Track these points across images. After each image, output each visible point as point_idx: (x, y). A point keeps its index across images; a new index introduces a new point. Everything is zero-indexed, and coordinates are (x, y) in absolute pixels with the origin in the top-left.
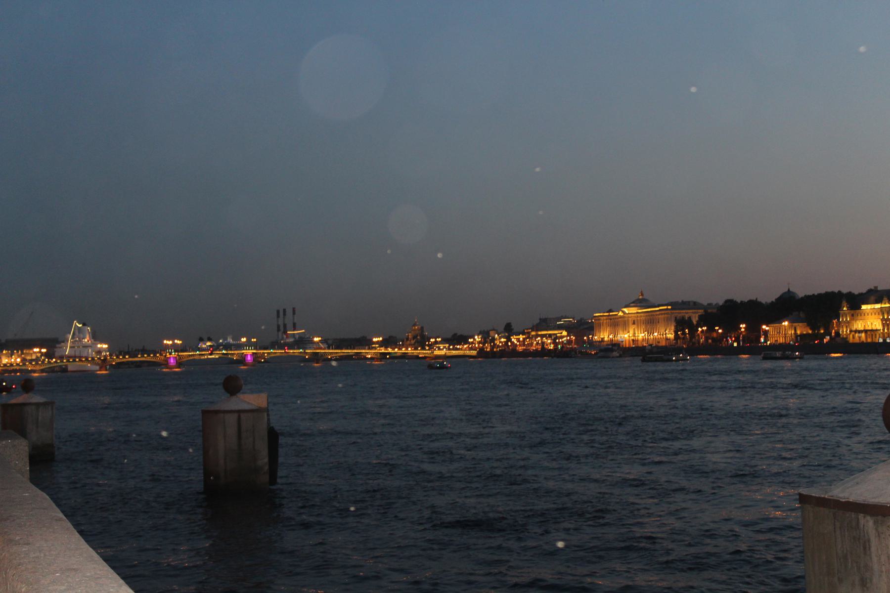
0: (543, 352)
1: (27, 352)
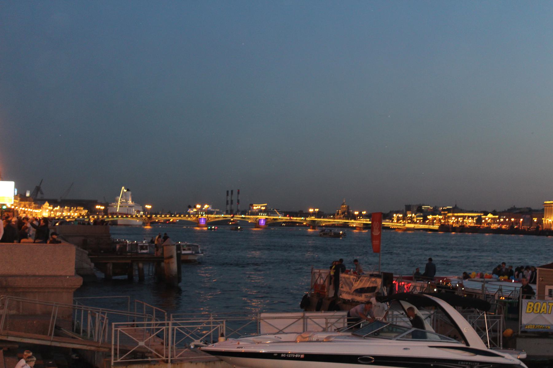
0: (463, 229)
1: (80, 209)
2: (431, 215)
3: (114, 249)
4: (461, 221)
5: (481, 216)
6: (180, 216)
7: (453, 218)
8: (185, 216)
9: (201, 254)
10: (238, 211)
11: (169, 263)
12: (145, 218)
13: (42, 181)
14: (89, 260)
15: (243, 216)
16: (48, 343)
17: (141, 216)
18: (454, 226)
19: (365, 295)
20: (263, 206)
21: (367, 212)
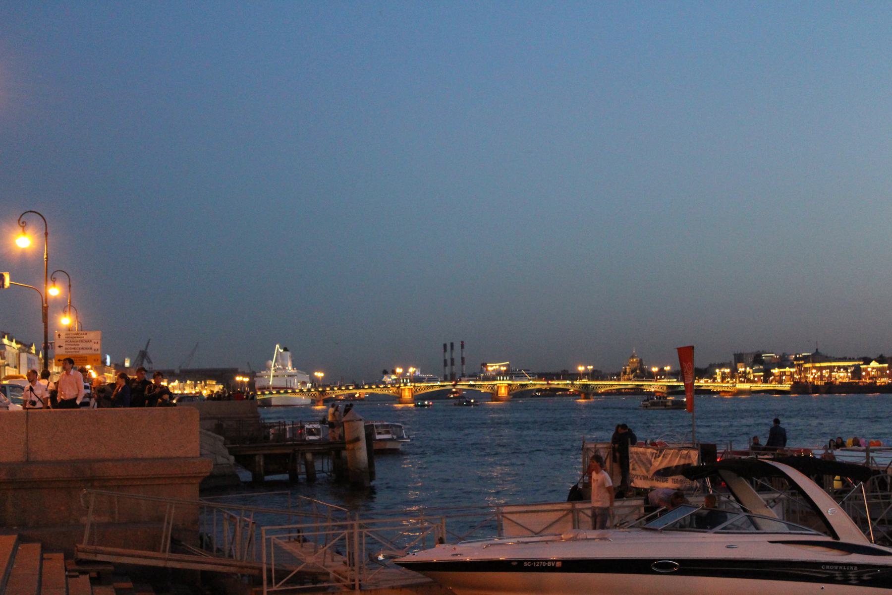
0: (831, 388)
1: (210, 383)
2: (776, 369)
3: (267, 438)
4: (827, 376)
5: (859, 365)
6: (370, 388)
7: (814, 371)
8: (377, 387)
9: (406, 439)
10: (463, 375)
11: (353, 449)
12: (314, 392)
13: (148, 343)
14: (226, 452)
15: (472, 383)
16: (161, 564)
17: (309, 390)
18: (815, 384)
19: (672, 479)
20: (503, 366)
21: (671, 367)
